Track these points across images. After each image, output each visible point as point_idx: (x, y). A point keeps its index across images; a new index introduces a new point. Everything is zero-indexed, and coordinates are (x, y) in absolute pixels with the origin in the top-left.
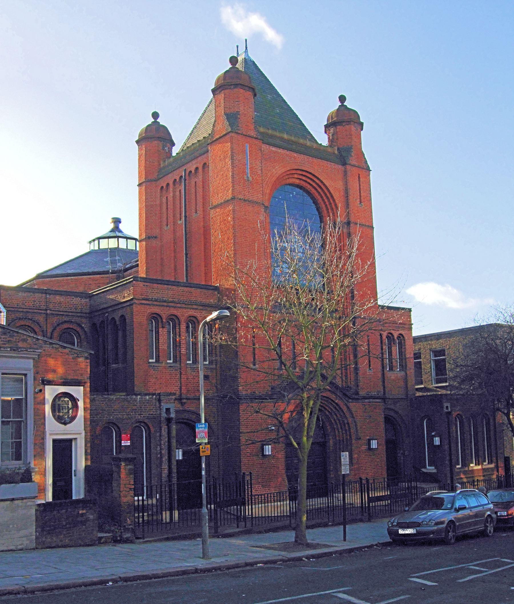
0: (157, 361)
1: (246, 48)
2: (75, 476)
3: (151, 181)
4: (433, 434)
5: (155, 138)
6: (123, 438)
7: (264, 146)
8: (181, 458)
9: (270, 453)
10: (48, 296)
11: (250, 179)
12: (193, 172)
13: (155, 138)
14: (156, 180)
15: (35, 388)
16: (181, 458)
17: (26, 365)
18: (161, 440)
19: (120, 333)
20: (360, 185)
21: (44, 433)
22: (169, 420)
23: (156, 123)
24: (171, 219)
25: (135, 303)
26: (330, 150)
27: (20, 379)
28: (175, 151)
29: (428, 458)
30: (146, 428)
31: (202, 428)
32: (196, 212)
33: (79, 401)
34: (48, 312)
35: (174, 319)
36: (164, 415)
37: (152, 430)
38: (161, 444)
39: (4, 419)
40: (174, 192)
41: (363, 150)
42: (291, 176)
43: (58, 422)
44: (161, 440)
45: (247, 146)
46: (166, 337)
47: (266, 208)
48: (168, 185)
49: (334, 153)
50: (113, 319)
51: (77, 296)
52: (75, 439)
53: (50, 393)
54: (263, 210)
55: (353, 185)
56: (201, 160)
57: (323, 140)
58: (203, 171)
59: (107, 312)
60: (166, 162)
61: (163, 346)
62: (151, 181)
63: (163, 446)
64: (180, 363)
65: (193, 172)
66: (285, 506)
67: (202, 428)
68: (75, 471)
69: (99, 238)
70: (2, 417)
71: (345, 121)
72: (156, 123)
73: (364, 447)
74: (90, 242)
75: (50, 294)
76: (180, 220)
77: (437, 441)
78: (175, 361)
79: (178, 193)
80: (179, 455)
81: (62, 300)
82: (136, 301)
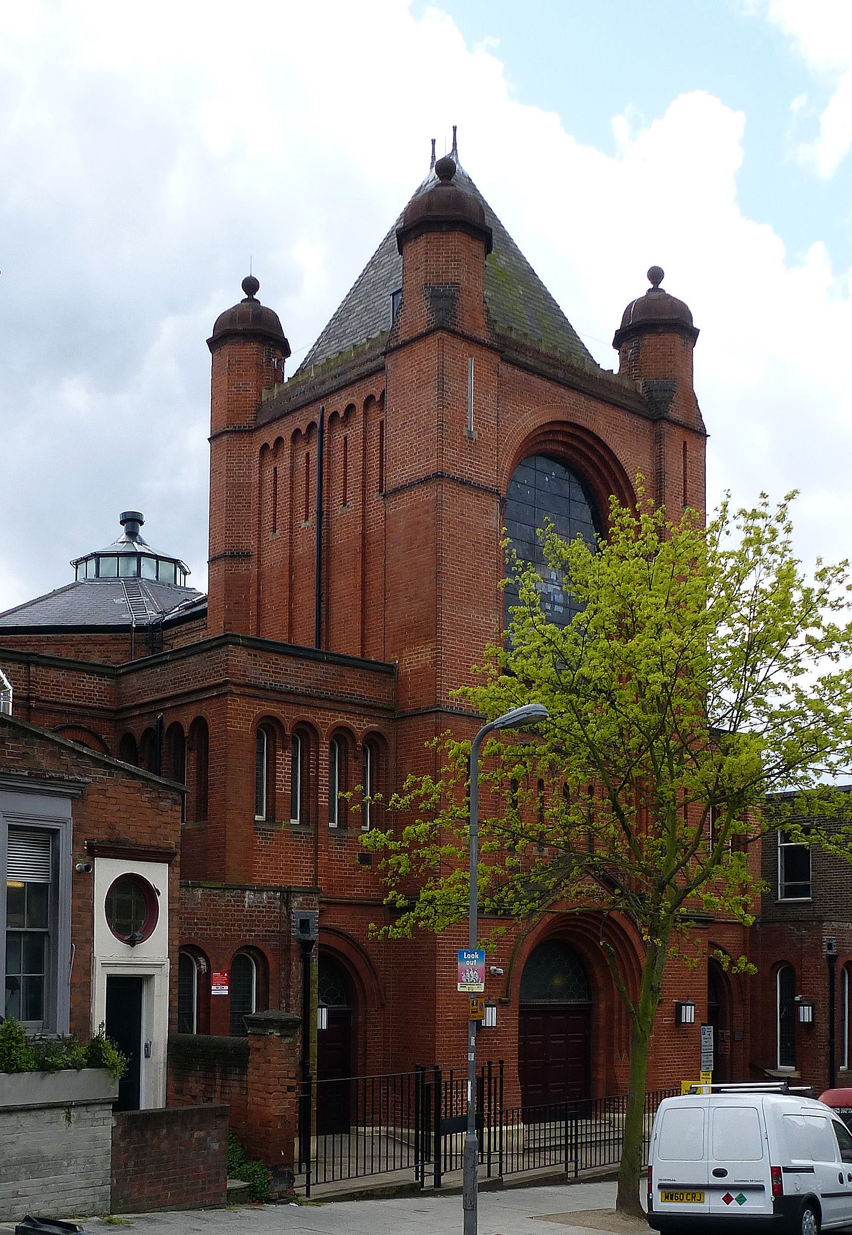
0: (271, 817)
1: (455, 144)
2: (147, 1056)
3: (239, 432)
4: (797, 998)
5: (247, 333)
6: (215, 979)
7: (502, 367)
8: (324, 1027)
9: (494, 1025)
10: (32, 669)
11: (475, 435)
12: (341, 414)
13: (247, 333)
14: (251, 431)
15: (75, 862)
16: (324, 1027)
17: (56, 810)
18: (290, 987)
19: (191, 760)
20: (685, 468)
21: (89, 959)
22: (306, 946)
23: (251, 300)
24: (284, 517)
25: (232, 693)
26: (627, 384)
27: (44, 837)
28: (291, 367)
29: (781, 1048)
30: (259, 959)
31: (471, 959)
32: (345, 504)
33: (159, 894)
34: (33, 704)
35: (306, 732)
36: (295, 932)
37: (272, 966)
38: (288, 996)
39: (10, 929)
40: (293, 457)
41: (699, 388)
42: (551, 437)
43: (119, 938)
44: (290, 987)
45: (471, 362)
46: (288, 769)
47: (503, 501)
48: (279, 441)
49: (636, 392)
50: (176, 726)
51: (91, 673)
52: (152, 976)
53: (107, 872)
54: (496, 506)
55: (673, 467)
56: (373, 387)
57: (608, 359)
58: (365, 414)
59: (161, 710)
60: (276, 391)
61: (283, 789)
62: (239, 432)
63: (292, 1001)
64: (317, 826)
65: (341, 414)
66: (515, 1133)
67: (471, 959)
68: (146, 1046)
69: (97, 556)
70: (8, 923)
71: (660, 326)
72: (251, 300)
73: (667, 1021)
74: (77, 563)
75: (37, 664)
76: (306, 519)
77: (806, 1014)
78: (304, 822)
79: (301, 461)
80: (322, 1019)
81: (61, 679)
82: (234, 689)
